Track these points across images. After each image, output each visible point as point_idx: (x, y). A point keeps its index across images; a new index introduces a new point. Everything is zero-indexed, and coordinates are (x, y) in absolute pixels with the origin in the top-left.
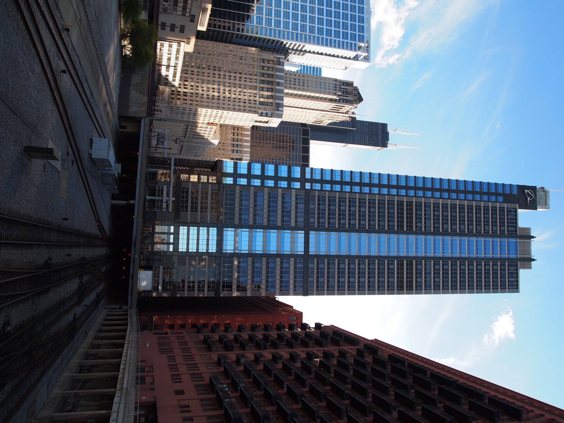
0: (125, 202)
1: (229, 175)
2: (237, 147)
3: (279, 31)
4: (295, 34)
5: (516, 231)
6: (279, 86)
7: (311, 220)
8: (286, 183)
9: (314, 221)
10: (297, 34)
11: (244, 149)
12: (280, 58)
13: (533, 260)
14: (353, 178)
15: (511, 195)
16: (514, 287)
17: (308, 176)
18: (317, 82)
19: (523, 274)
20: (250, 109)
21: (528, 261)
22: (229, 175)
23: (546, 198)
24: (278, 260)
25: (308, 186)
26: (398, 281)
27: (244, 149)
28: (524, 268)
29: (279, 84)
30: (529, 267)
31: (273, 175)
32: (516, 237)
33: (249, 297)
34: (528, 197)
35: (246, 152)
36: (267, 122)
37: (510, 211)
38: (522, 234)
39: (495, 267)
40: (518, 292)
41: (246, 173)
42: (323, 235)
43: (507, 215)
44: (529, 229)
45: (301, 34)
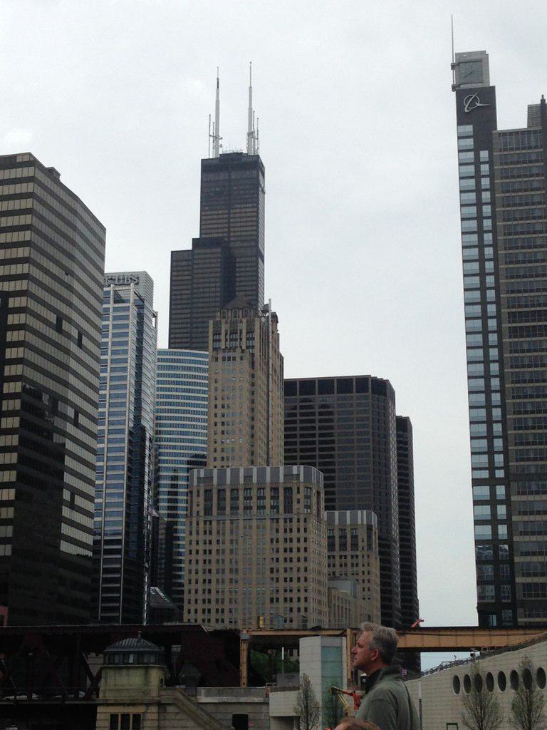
1: (495, 531)
3: (110, 414)
4: (114, 366)
5: (535, 132)
8: (499, 507)
10: (110, 432)
11: (348, 522)
15: (475, 136)
17: (485, 474)
22: (495, 531)
27: (348, 522)
31: (490, 526)
37: (505, 144)
41: (489, 507)
44: (530, 108)
45: (110, 423)
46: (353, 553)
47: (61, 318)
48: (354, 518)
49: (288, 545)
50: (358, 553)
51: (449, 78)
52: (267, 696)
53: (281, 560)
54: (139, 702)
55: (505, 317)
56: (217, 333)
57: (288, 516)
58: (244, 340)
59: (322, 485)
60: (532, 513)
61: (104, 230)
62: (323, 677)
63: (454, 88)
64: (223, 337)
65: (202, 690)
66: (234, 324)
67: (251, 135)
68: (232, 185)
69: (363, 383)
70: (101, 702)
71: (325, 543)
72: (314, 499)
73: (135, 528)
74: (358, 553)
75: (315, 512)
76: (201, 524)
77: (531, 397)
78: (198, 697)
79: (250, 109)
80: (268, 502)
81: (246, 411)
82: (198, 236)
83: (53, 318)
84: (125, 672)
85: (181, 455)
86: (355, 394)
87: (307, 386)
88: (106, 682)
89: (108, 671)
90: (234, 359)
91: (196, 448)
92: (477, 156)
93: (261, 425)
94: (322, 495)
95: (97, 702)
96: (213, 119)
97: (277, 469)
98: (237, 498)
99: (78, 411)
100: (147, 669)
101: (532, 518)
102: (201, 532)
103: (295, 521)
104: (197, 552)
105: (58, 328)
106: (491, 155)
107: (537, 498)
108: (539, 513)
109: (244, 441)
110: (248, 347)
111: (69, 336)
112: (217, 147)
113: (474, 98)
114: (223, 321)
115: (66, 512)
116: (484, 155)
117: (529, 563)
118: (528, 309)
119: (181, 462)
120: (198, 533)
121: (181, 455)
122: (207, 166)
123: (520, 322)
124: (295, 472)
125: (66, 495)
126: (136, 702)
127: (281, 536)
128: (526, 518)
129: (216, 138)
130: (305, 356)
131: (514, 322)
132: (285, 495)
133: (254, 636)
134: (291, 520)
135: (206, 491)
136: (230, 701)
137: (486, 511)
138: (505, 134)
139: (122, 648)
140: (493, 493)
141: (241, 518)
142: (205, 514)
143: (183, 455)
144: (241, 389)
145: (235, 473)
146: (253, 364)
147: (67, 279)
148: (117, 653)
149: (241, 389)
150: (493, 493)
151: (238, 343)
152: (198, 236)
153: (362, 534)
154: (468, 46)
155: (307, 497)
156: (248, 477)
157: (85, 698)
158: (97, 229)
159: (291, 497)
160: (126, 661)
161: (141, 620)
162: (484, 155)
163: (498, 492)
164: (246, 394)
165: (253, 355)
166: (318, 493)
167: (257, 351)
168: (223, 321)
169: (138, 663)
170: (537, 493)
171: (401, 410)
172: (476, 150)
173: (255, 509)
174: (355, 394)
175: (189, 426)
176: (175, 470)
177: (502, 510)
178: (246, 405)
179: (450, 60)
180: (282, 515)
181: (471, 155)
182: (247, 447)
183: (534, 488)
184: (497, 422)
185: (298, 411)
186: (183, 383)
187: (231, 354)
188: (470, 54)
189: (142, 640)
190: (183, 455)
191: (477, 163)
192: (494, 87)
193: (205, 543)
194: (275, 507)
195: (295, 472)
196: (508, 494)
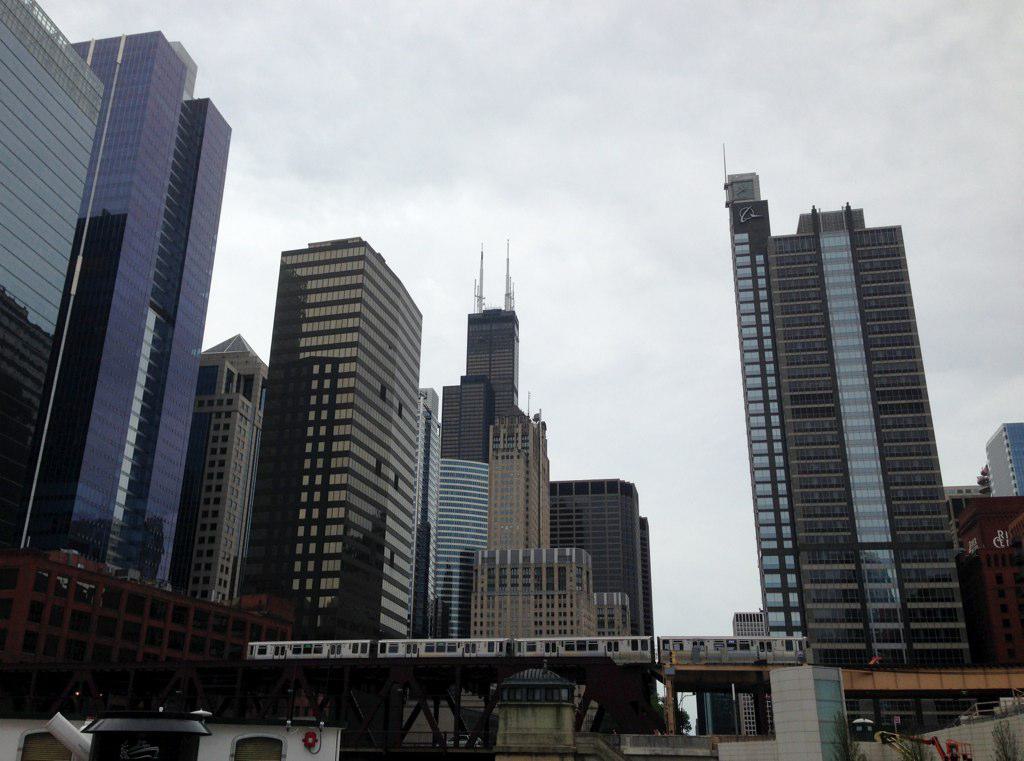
2: (517, 577)
6: (494, 558)
7: (841, 541)
12: (483, 558)
14: (765, 480)
15: (751, 243)
17: (774, 545)
18: (502, 491)
19: (871, 222)
24: (907, 585)
25: (788, 545)
28: (862, 220)
30: (860, 212)
32: (817, 237)
33: (963, 604)
37: (781, 247)
40: (900, 228)
42: (860, 523)
47: (380, 461)
48: (610, 600)
49: (562, 619)
51: (722, 196)
52: (714, 747)
54: (551, 751)
56: (497, 436)
58: (520, 443)
59: (590, 566)
60: (824, 582)
61: (421, 316)
62: (820, 722)
65: (628, 738)
66: (510, 428)
67: (509, 296)
68: (493, 334)
70: (501, 750)
71: (594, 617)
72: (584, 577)
73: (421, 606)
75: (585, 589)
76: (485, 598)
77: (817, 472)
78: (622, 747)
79: (508, 278)
81: (522, 501)
82: (464, 374)
83: (373, 462)
84: (529, 711)
85: (455, 547)
87: (565, 487)
88: (506, 724)
89: (508, 709)
90: (512, 457)
91: (468, 542)
92: (753, 260)
93: (534, 515)
94: (591, 575)
95: (495, 750)
96: (478, 283)
97: (547, 554)
99: (398, 476)
100: (559, 707)
101: (824, 586)
102: (485, 606)
104: (482, 624)
105: (383, 396)
106: (766, 259)
107: (828, 567)
108: (830, 581)
109: (520, 527)
110: (523, 448)
111: (387, 479)
112: (480, 305)
113: (746, 208)
114: (502, 426)
115: (387, 569)
116: (760, 258)
117: (823, 630)
119: (455, 553)
120: (482, 607)
121: (455, 547)
122: (473, 320)
123: (810, 403)
124: (568, 554)
125: (387, 553)
126: (546, 751)
128: (818, 586)
129: (480, 298)
130: (566, 464)
132: (552, 579)
133: (677, 672)
134: (565, 596)
135: (489, 570)
136: (666, 754)
137: (775, 580)
138: (779, 239)
139: (524, 680)
140: (782, 562)
141: (521, 594)
142: (489, 590)
144: (518, 482)
145: (515, 554)
146: (527, 462)
147: (390, 352)
148: (520, 686)
149: (518, 482)
150: (782, 562)
151: (515, 444)
152: (464, 374)
153: (618, 613)
154: (740, 169)
155: (579, 576)
156: (526, 558)
157: (466, 747)
158: (417, 317)
159: (565, 576)
160: (550, 697)
162: (760, 258)
164: (522, 487)
165: (527, 455)
166: (588, 573)
167: (531, 451)
168: (502, 426)
169: (547, 700)
170: (827, 562)
171: (642, 513)
172: (752, 254)
175: (463, 524)
178: (522, 496)
179: (722, 182)
180: (557, 592)
182: (523, 533)
183: (824, 558)
186: (457, 487)
187: (510, 453)
188: (742, 175)
189: (549, 672)
191: (753, 265)
192: (766, 202)
193: (488, 616)
194: (538, 586)
195: (568, 554)
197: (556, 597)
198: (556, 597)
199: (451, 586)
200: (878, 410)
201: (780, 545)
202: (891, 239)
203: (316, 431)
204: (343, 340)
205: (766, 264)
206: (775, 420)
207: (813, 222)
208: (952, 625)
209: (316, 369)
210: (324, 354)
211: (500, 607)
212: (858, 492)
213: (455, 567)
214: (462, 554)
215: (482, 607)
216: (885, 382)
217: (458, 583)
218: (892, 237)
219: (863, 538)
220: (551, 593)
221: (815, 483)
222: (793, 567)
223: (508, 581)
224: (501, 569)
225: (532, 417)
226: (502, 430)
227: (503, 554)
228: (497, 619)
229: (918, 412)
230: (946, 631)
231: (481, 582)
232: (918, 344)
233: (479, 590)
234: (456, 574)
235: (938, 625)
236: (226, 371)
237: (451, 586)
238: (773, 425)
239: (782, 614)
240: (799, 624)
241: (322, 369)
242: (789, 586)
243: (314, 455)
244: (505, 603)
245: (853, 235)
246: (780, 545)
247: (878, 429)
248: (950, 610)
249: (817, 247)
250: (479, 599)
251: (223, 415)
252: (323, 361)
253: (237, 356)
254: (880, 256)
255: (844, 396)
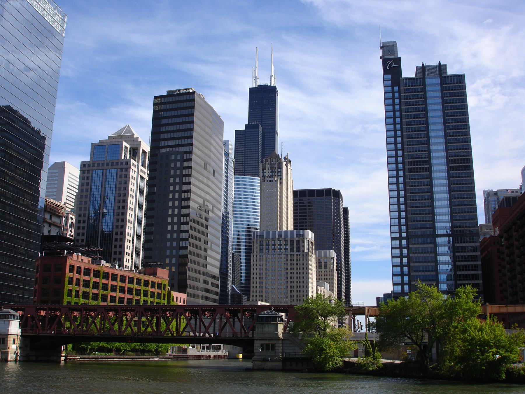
0: (391, 361)
5: (420, 78)
7: (428, 233)
9: (429, 231)
11: (323, 256)
12: (257, 236)
13: (440, 63)
15: (392, 80)
16: (460, 79)
17: (397, 235)
19: (451, 71)
20: (305, 259)
21: (441, 68)
23: (389, 46)
26: (465, 170)
27: (323, 256)
28: (446, 70)
29: (274, 233)
30: (445, 66)
32: (424, 79)
34: (391, 66)
35: (325, 254)
36: (312, 243)
37: (406, 84)
38: (422, 74)
39: (449, 101)
43: (409, 86)
44: (417, 68)
46: (325, 270)
50: (327, 270)
53: (295, 273)
55: (407, 163)
57: (298, 253)
58: (277, 172)
63: (381, 58)
64: (267, 171)
69: (328, 192)
74: (327, 270)
76: (258, 256)
80: (289, 247)
86: (324, 197)
92: (393, 89)
98: (263, 245)
103: (301, 255)
105: (205, 168)
111: (209, 172)
116: (396, 88)
118: (417, 160)
120: (257, 261)
127: (289, 262)
131: (411, 165)
135: (260, 241)
138: (406, 79)
142: (260, 252)
143: (243, 224)
150: (401, 243)
161: (227, 302)
162: (396, 88)
163: (403, 244)
172: (393, 86)
173: (271, 250)
174: (324, 197)
176: (239, 231)
177: (405, 251)
179: (379, 45)
181: (390, 89)
184: (403, 211)
185: (307, 208)
190: (243, 224)
191: (393, 92)
192: (400, 58)
195: (301, 233)
196: (408, 244)
197: (295, 256)
198: (295, 256)
199: (241, 242)
200: (450, 169)
201: (400, 235)
202: (460, 81)
203: (174, 204)
204: (182, 99)
205: (399, 92)
206: (398, 120)
207: (422, 70)
208: (475, 272)
209: (173, 157)
210: (177, 149)
211: (266, 260)
212: (435, 174)
213: (243, 231)
214: (246, 228)
215: (257, 261)
216: (453, 154)
217: (245, 244)
218: (460, 79)
219: (439, 232)
220: (292, 253)
221: (414, 136)
222: (406, 264)
223: (270, 247)
224: (266, 241)
225: (283, 158)
226: (267, 165)
227: (268, 233)
228: (264, 267)
229: (468, 170)
230: (473, 275)
231: (256, 247)
232: (469, 122)
233: (255, 252)
234: (243, 239)
235: (469, 272)
236: (124, 146)
237: (241, 242)
238: (396, 116)
239: (399, 259)
240: (407, 282)
241: (176, 157)
242: (404, 273)
243: (174, 200)
244: (269, 258)
245: (441, 78)
246: (400, 235)
247: (442, 97)
248: (476, 275)
249: (424, 84)
250: (255, 257)
251: (124, 170)
252: (176, 153)
253: (128, 137)
254: (453, 89)
255: (434, 161)
